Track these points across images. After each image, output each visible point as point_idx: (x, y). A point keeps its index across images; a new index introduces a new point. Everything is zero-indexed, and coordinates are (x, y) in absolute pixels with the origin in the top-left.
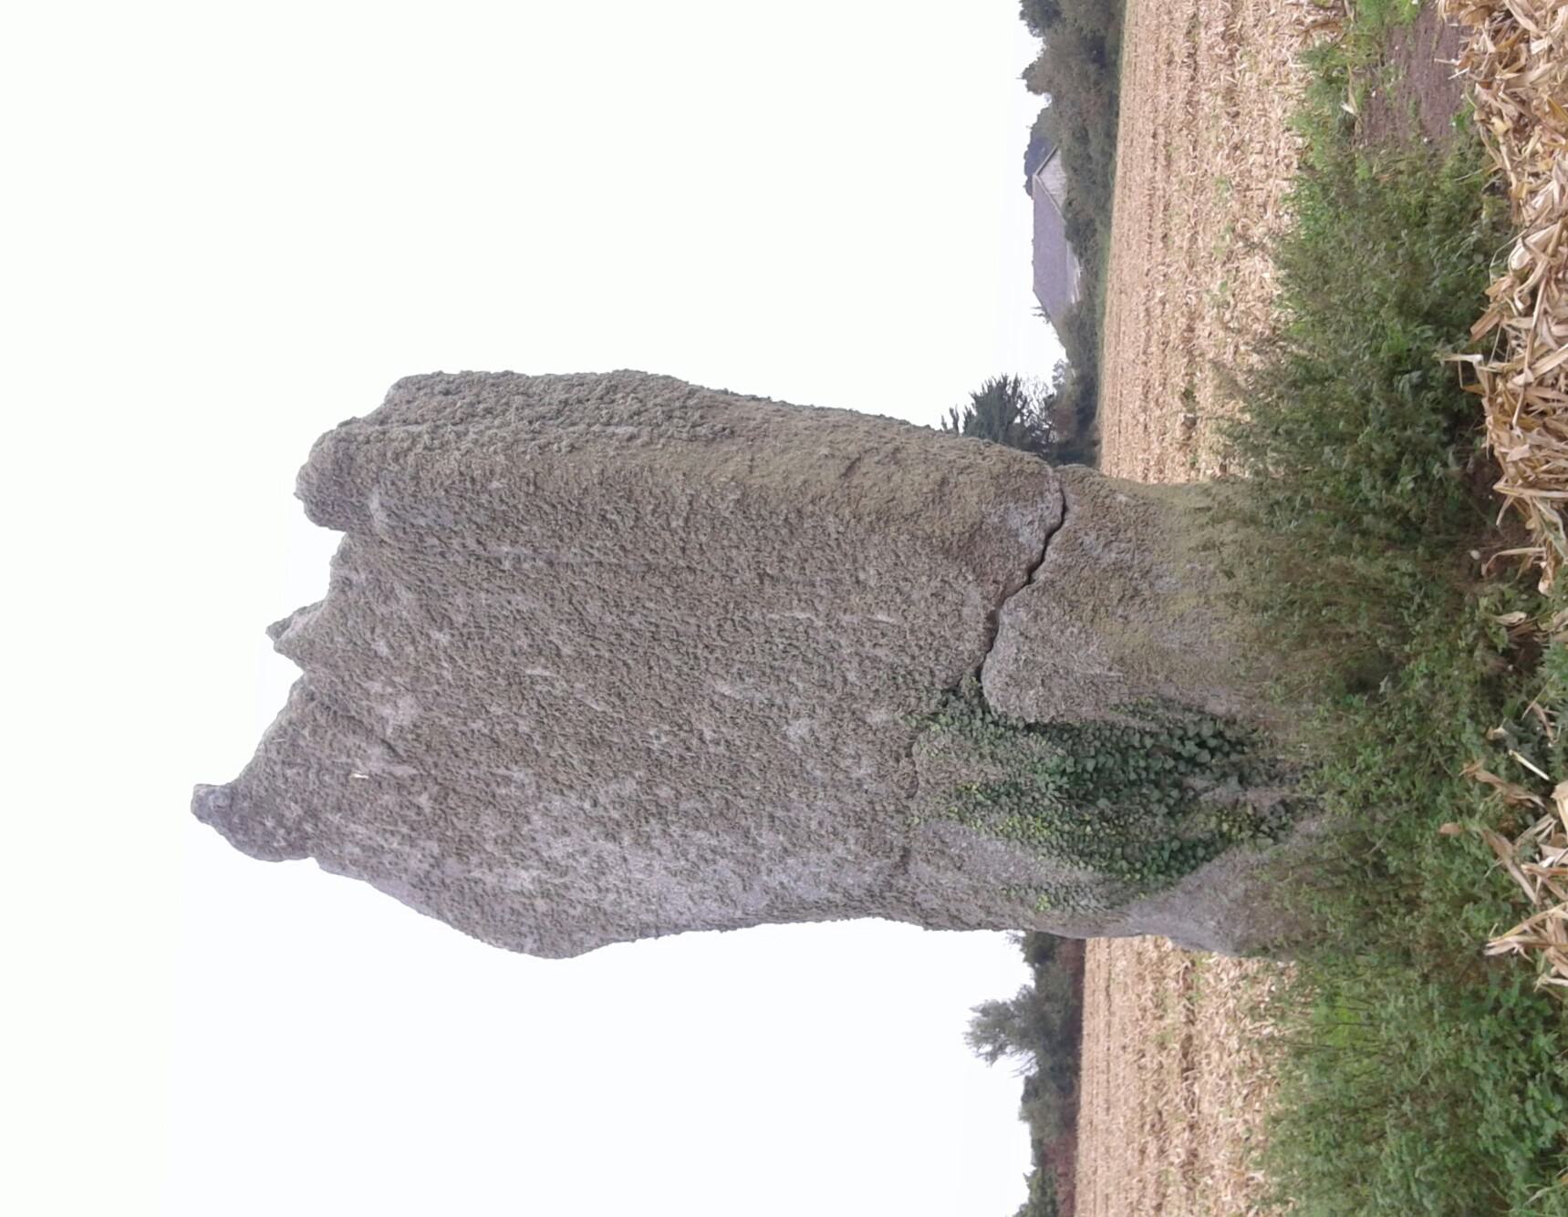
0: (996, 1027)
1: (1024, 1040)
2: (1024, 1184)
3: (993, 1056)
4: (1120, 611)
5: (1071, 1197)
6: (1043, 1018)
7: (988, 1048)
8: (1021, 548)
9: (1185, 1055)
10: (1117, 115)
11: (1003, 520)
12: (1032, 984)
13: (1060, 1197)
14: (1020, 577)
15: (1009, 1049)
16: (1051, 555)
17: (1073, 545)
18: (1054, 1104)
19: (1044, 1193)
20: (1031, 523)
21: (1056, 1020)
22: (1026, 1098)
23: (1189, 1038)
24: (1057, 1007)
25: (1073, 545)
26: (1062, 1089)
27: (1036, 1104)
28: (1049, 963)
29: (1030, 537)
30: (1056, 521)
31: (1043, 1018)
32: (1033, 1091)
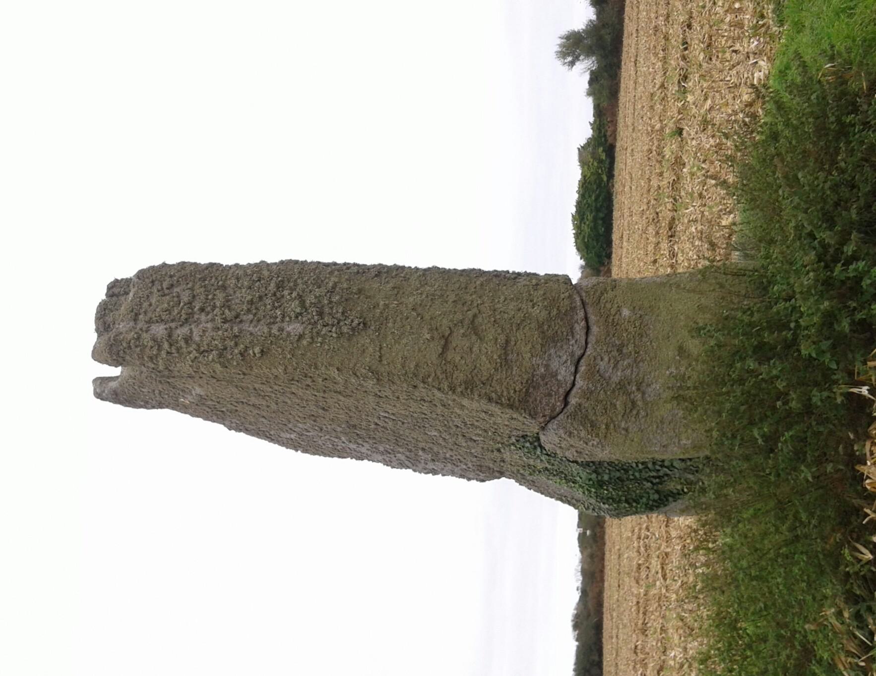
0: (573, 46)
1: (589, 52)
2: (590, 127)
3: (572, 63)
4: (623, 425)
5: (615, 132)
6: (600, 38)
7: (570, 59)
8: (559, 384)
9: (670, 229)
10: (604, 544)
11: (547, 366)
12: (594, 17)
13: (609, 133)
14: (559, 405)
15: (582, 57)
16: (580, 383)
17: (593, 373)
18: (606, 89)
19: (600, 132)
20: (566, 362)
21: (608, 38)
22: (591, 82)
23: (673, 219)
24: (608, 31)
25: (593, 373)
26: (611, 76)
27: (597, 86)
28: (604, 5)
29: (564, 374)
30: (582, 351)
31: (600, 38)
32: (594, 79)
